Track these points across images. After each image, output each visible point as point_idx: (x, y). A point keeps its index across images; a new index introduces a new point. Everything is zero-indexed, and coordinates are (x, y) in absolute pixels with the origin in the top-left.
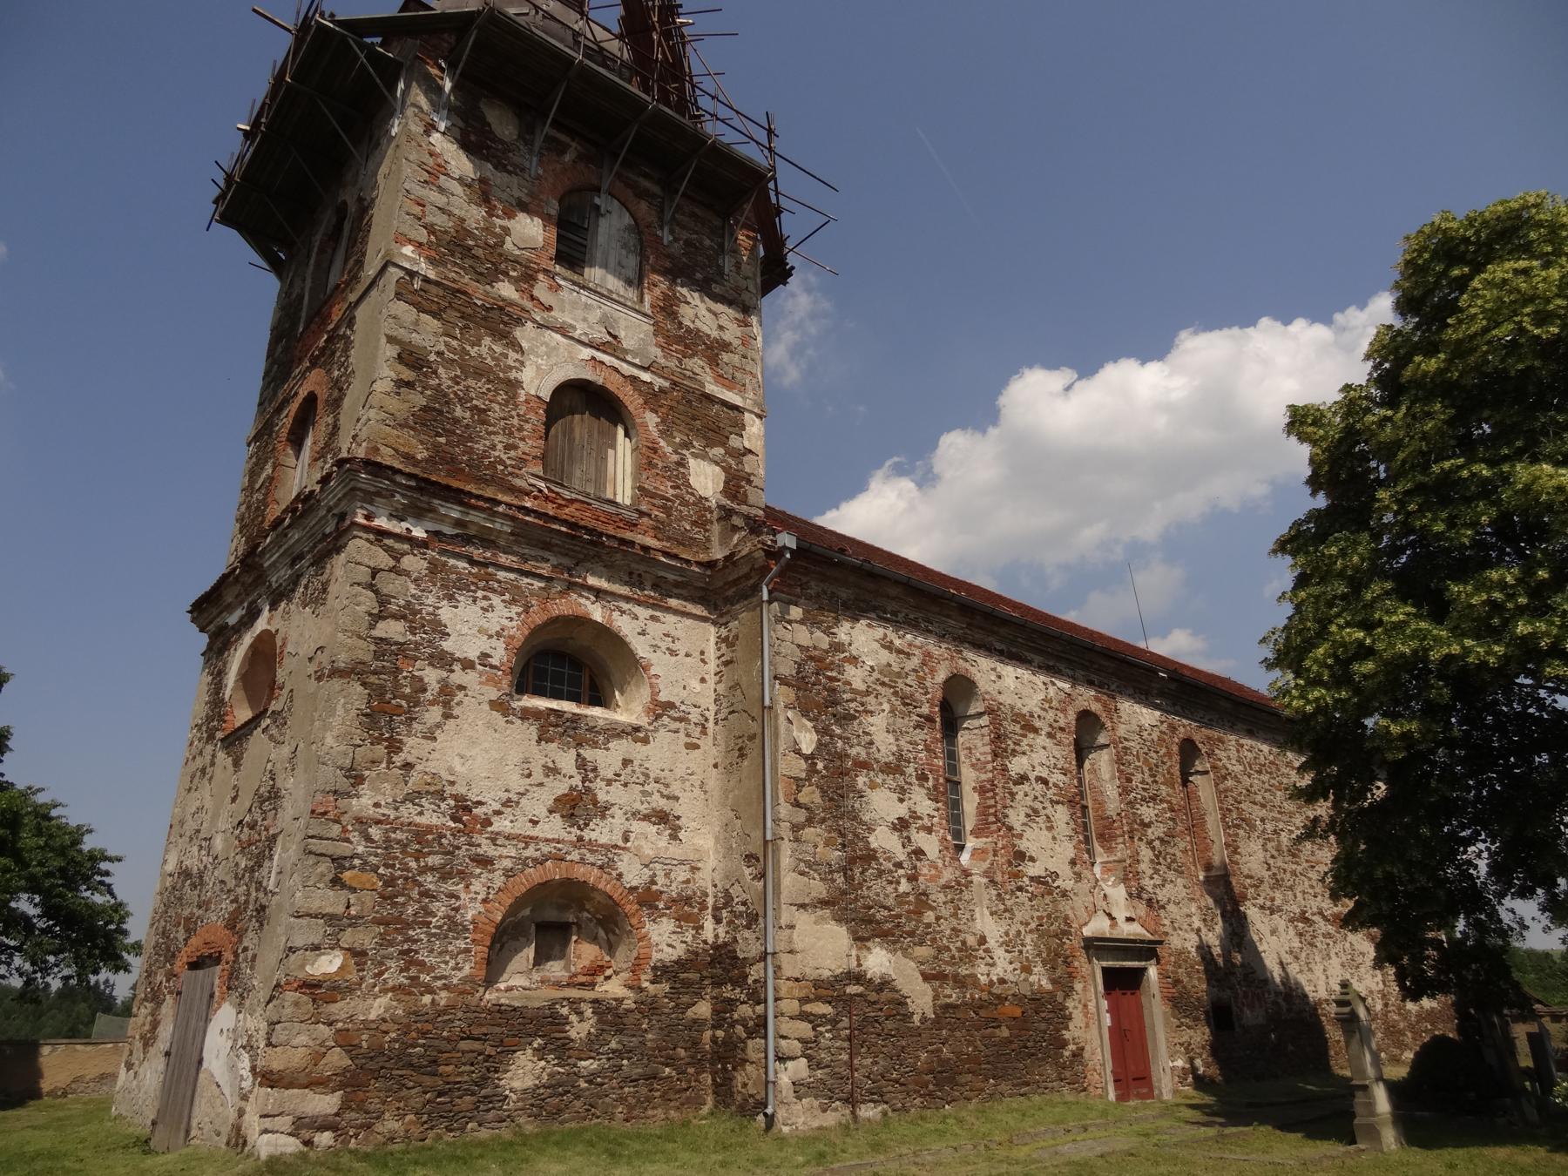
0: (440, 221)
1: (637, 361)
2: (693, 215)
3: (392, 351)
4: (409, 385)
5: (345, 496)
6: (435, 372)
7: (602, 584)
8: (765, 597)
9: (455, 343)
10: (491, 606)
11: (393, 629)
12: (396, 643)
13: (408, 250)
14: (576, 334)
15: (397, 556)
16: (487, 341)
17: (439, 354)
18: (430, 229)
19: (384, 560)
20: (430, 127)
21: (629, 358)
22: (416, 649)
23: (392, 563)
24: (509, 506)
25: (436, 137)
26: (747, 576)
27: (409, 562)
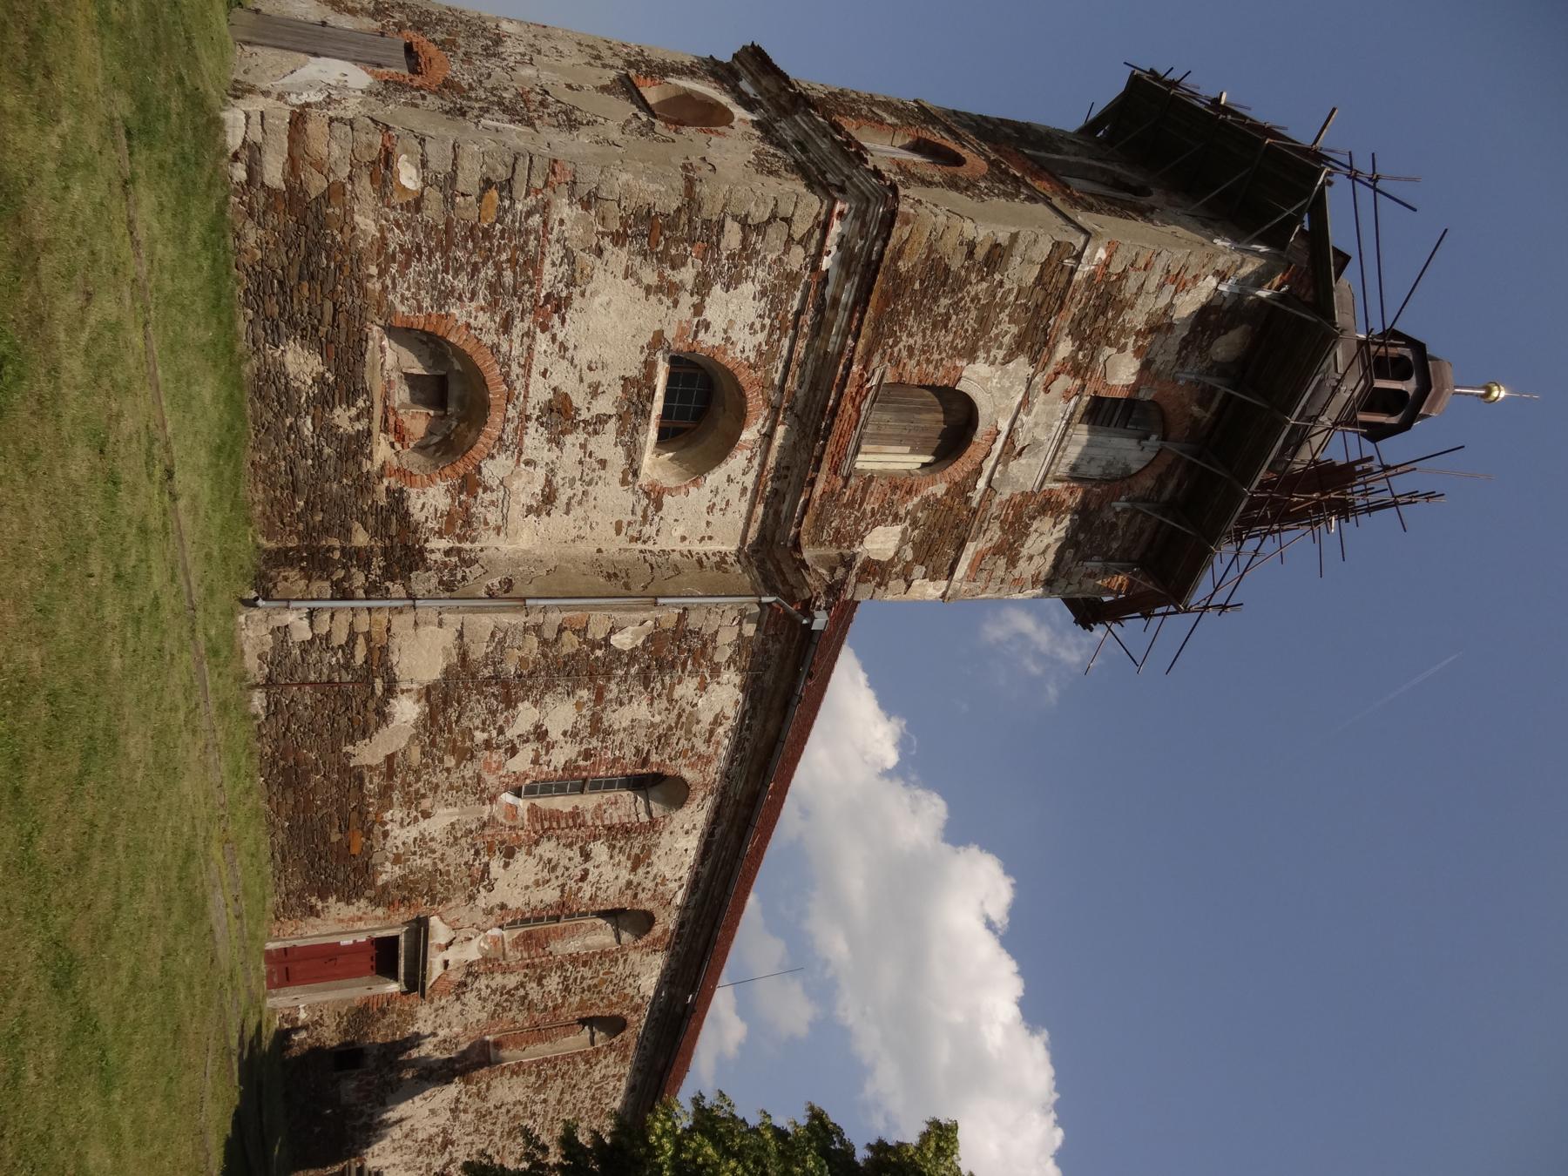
1: (996, 475)
3: (1003, 237)
4: (970, 254)
5: (862, 192)
6: (983, 279)
9: (1012, 298)
10: (755, 332)
12: (719, 241)
14: (1022, 416)
15: (804, 241)
16: (1014, 329)
17: (1001, 283)
19: (799, 230)
21: (1000, 467)
22: (713, 260)
23: (797, 237)
24: (853, 350)
25: (1212, 282)
26: (785, 582)
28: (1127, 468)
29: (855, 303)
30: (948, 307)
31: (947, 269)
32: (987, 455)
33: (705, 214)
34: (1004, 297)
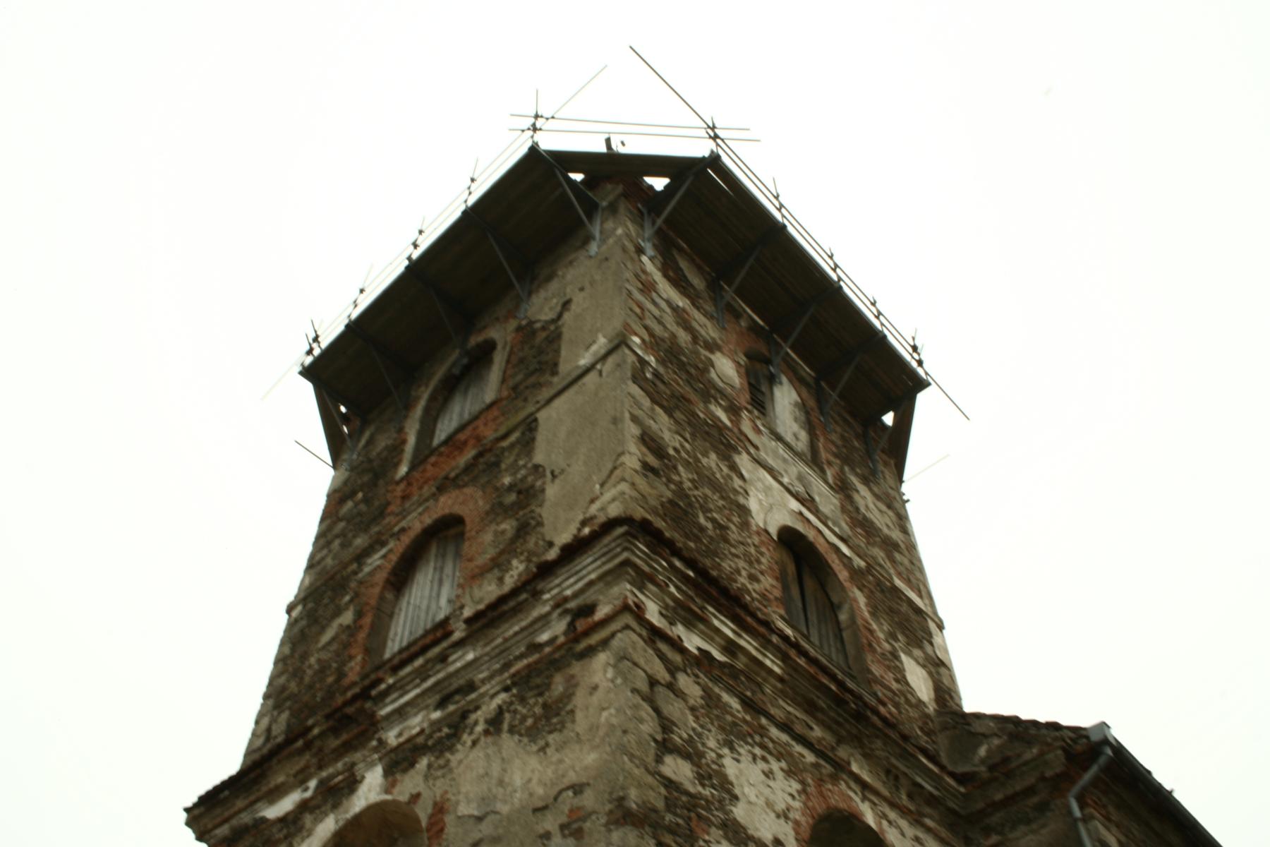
0: (658, 329)
1: (836, 529)
2: (840, 415)
3: (635, 430)
4: (653, 470)
5: (600, 578)
6: (675, 468)
7: (866, 777)
8: (1077, 813)
9: (687, 445)
10: (771, 772)
11: (678, 769)
12: (687, 793)
13: (637, 340)
14: (786, 480)
15: (672, 669)
16: (713, 456)
17: (675, 449)
18: (652, 334)
19: (662, 674)
20: (640, 251)
21: (830, 524)
22: (708, 809)
23: (667, 677)
24: (785, 638)
25: (645, 259)
26: (1030, 791)
27: (684, 681)
28: (796, 405)
29: (736, 619)
30: (707, 519)
31: (671, 501)
32: (820, 532)
33: (660, 804)
34: (687, 452)
